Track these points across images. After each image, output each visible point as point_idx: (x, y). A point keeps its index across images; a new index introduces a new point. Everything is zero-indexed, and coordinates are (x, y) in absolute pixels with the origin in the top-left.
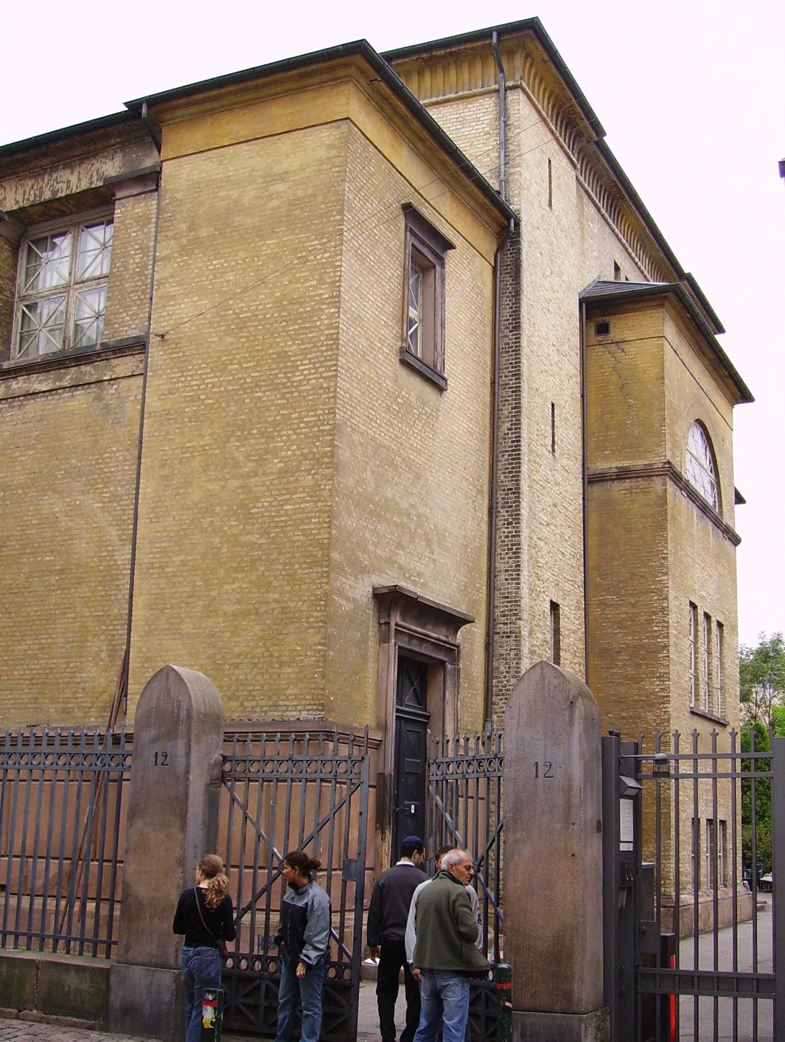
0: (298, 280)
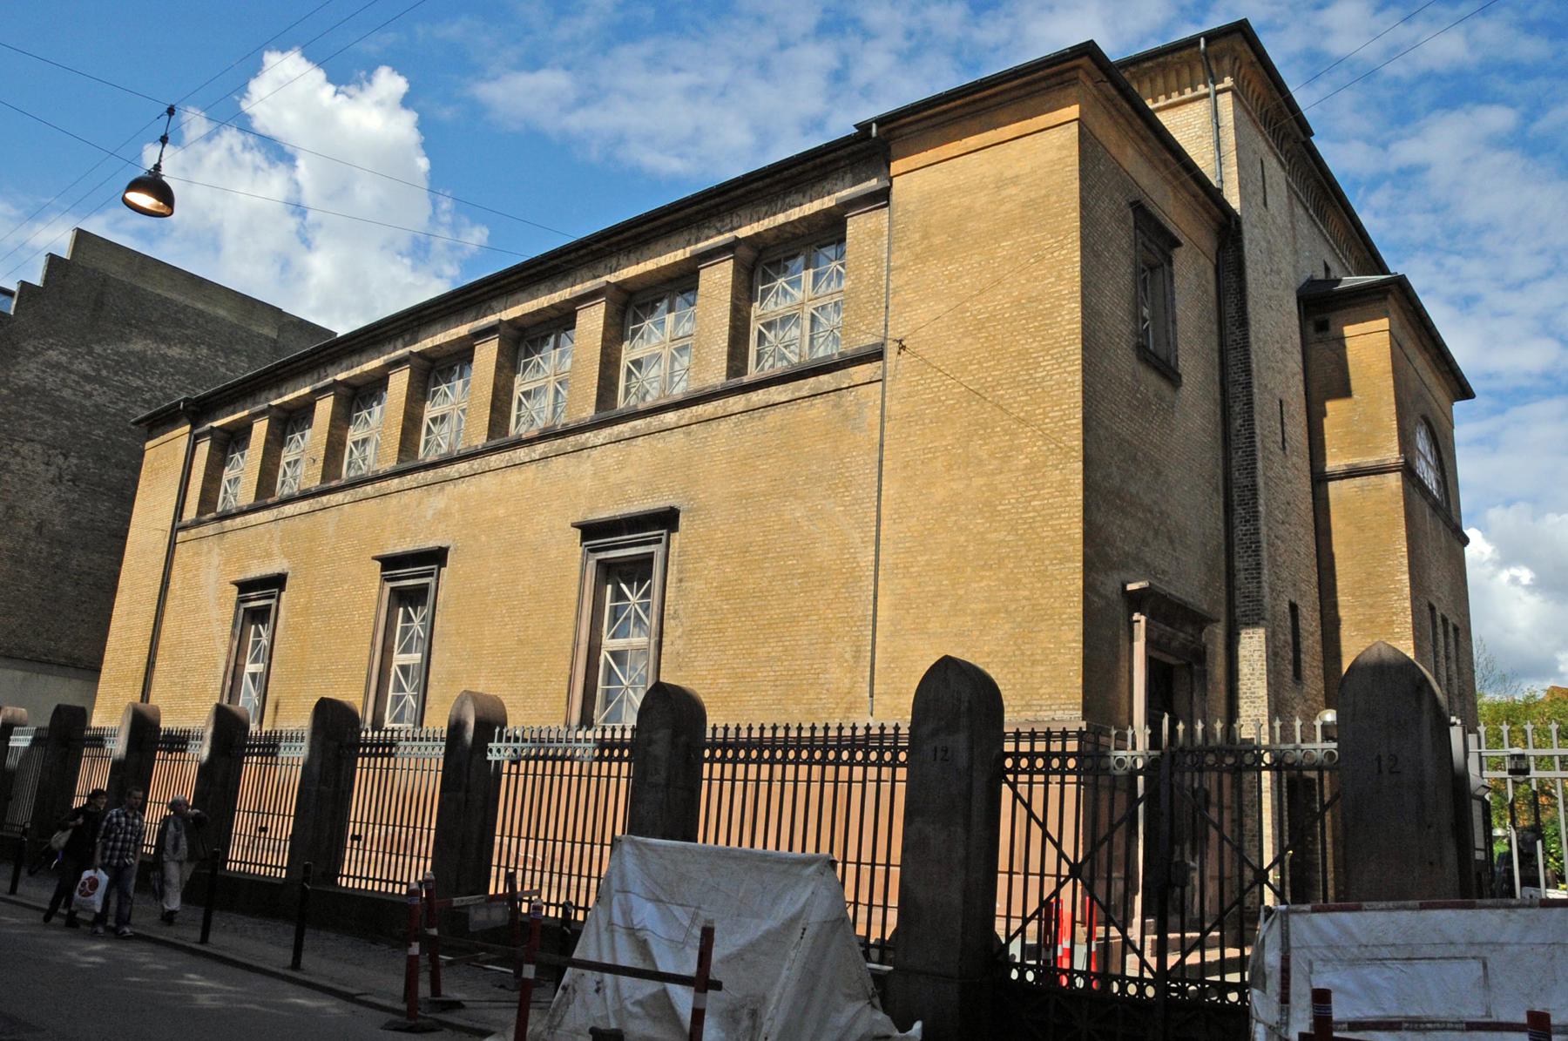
0: (1036, 279)
